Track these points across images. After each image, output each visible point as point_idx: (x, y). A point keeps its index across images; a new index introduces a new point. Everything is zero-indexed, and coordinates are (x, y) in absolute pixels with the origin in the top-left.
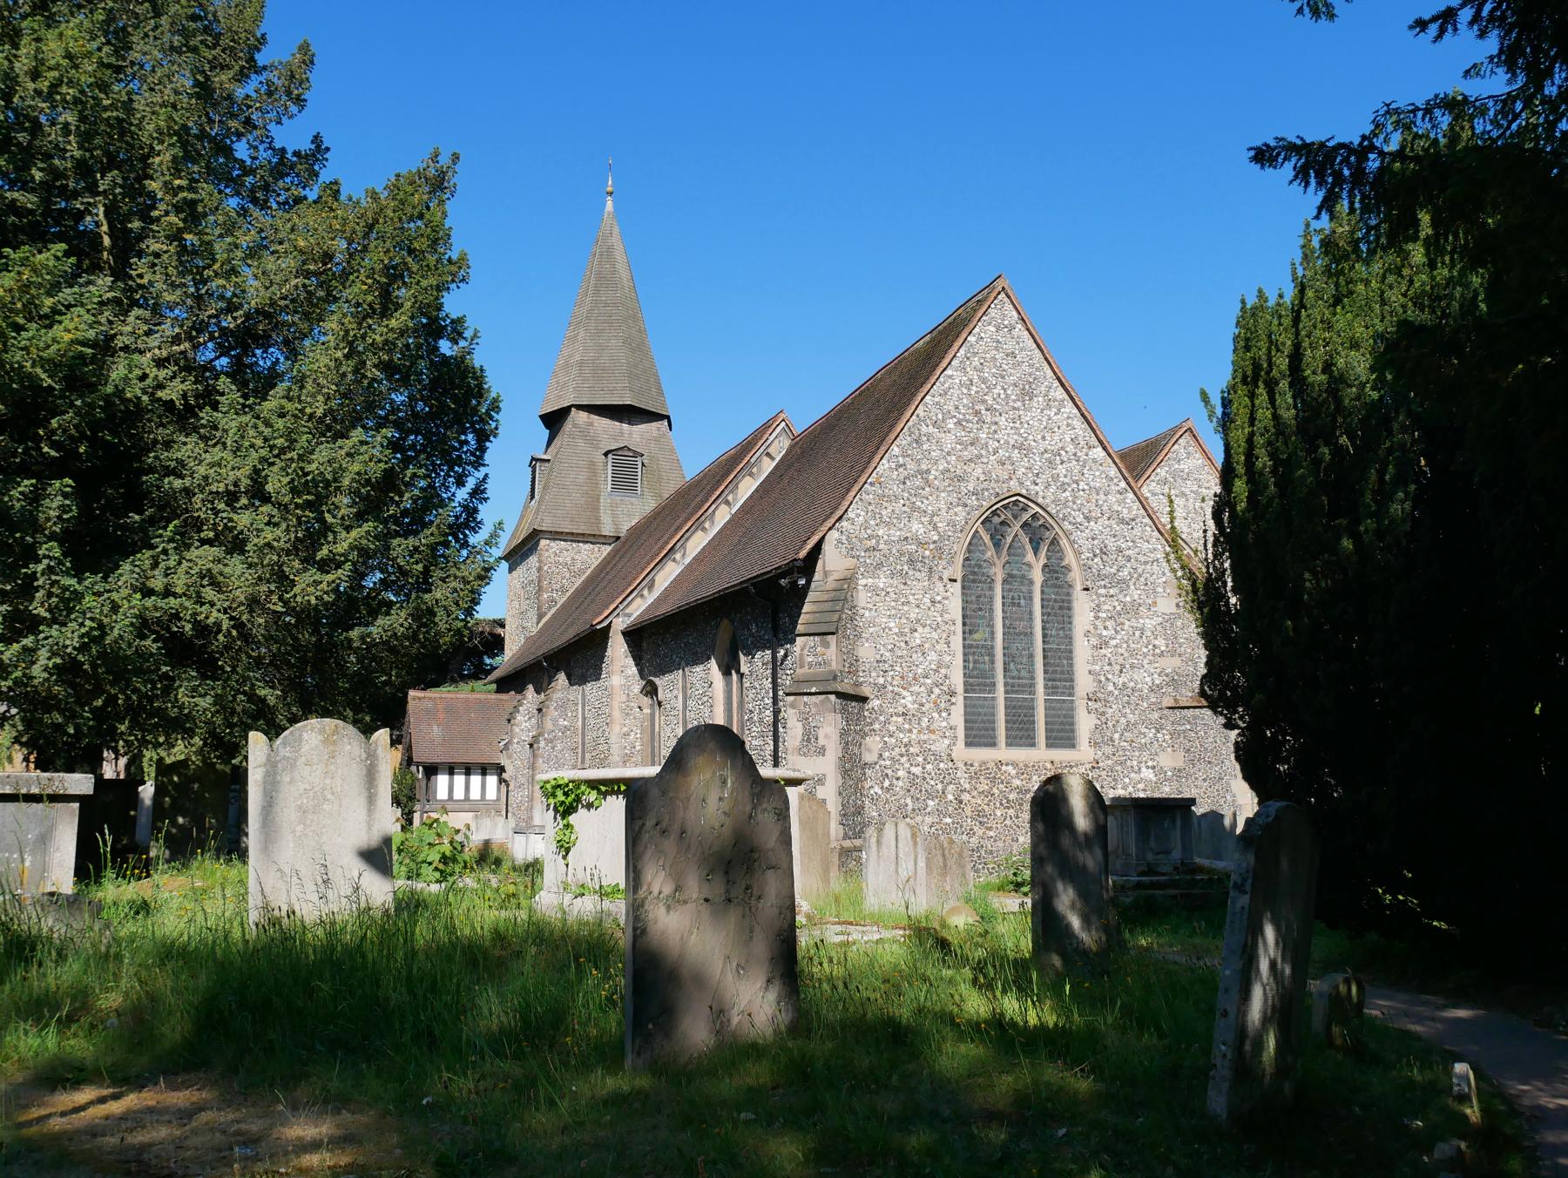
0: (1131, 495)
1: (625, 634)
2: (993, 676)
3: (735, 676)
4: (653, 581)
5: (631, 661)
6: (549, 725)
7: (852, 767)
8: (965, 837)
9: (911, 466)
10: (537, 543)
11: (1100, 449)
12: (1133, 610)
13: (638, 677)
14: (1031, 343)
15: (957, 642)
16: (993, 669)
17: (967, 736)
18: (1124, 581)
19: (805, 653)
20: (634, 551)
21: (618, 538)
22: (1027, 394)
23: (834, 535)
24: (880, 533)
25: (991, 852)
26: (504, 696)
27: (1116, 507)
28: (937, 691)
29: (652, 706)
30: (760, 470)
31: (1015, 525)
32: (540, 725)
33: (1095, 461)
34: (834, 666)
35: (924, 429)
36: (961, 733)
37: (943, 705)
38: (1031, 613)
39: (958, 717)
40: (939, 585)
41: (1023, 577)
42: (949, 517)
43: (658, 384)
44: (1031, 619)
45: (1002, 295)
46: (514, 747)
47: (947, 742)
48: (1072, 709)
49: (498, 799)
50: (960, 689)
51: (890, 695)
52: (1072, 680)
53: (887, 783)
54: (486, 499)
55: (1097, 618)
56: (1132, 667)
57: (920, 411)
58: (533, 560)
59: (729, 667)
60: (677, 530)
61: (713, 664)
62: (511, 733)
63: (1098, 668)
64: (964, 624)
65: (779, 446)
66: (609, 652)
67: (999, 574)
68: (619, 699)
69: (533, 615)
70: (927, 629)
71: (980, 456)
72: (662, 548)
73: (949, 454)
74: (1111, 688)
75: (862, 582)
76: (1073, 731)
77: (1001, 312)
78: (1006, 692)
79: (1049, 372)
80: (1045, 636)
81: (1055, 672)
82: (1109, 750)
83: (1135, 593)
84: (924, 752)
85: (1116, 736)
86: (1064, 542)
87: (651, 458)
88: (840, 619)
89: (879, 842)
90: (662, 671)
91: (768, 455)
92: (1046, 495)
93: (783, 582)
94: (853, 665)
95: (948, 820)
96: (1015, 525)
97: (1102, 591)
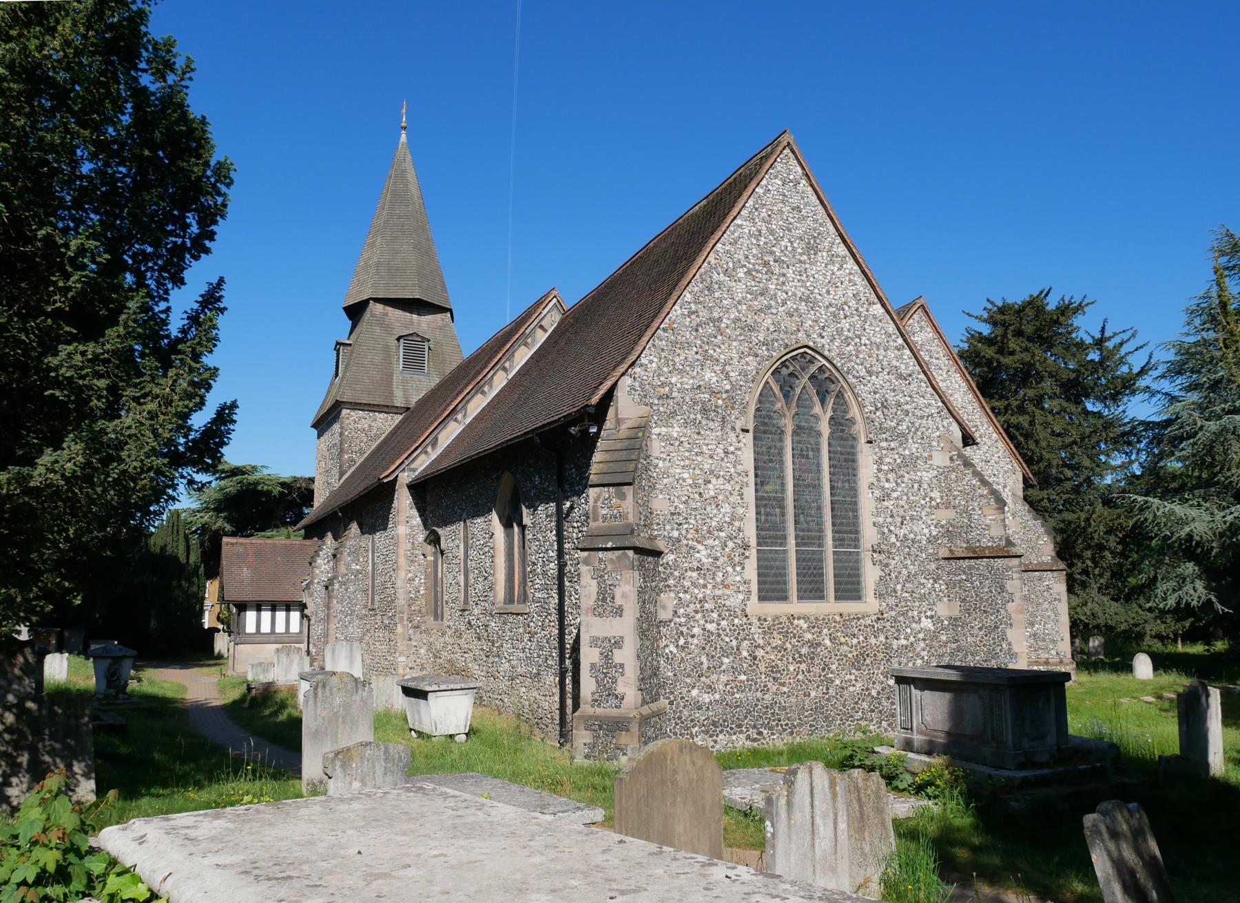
0: (907, 352)
2: (784, 529)
3: (516, 528)
4: (436, 439)
5: (415, 513)
7: (649, 627)
8: (759, 694)
9: (704, 314)
11: (879, 306)
12: (910, 463)
13: (422, 528)
14: (814, 199)
15: (750, 494)
16: (784, 522)
17: (760, 590)
18: (903, 435)
19: (597, 504)
20: (419, 419)
21: (408, 409)
22: (812, 249)
23: (626, 381)
24: (674, 380)
25: (785, 708)
26: (308, 542)
27: (894, 363)
28: (730, 544)
29: (435, 553)
30: (534, 341)
31: (803, 377)
32: (335, 569)
33: (874, 317)
34: (631, 519)
35: (715, 276)
36: (754, 587)
37: (737, 559)
38: (819, 465)
39: (751, 571)
40: (732, 436)
41: (811, 428)
42: (740, 367)
43: (441, 276)
44: (819, 471)
45: (787, 151)
47: (741, 597)
48: (858, 561)
49: (301, 632)
50: (753, 542)
51: (684, 550)
52: (857, 532)
53: (682, 642)
54: (222, 310)
55: (880, 470)
56: (912, 519)
57: (711, 258)
58: (336, 427)
59: (511, 520)
60: (460, 392)
61: (494, 517)
63: (881, 520)
64: (756, 476)
65: (551, 320)
67: (788, 425)
68: (405, 546)
69: (335, 472)
70: (721, 481)
71: (770, 307)
72: (445, 409)
73: (739, 303)
74: (893, 539)
75: (656, 431)
76: (859, 583)
77: (786, 167)
78: (797, 545)
79: (832, 228)
80: (832, 488)
81: (842, 524)
82: (892, 601)
83: (913, 447)
84: (719, 608)
85: (899, 587)
86: (849, 395)
87: (437, 343)
88: (636, 468)
89: (789, 804)
90: (445, 522)
91: (541, 327)
92: (832, 348)
93: (573, 430)
94: (648, 516)
95: (743, 677)
96: (803, 377)
97: (884, 444)
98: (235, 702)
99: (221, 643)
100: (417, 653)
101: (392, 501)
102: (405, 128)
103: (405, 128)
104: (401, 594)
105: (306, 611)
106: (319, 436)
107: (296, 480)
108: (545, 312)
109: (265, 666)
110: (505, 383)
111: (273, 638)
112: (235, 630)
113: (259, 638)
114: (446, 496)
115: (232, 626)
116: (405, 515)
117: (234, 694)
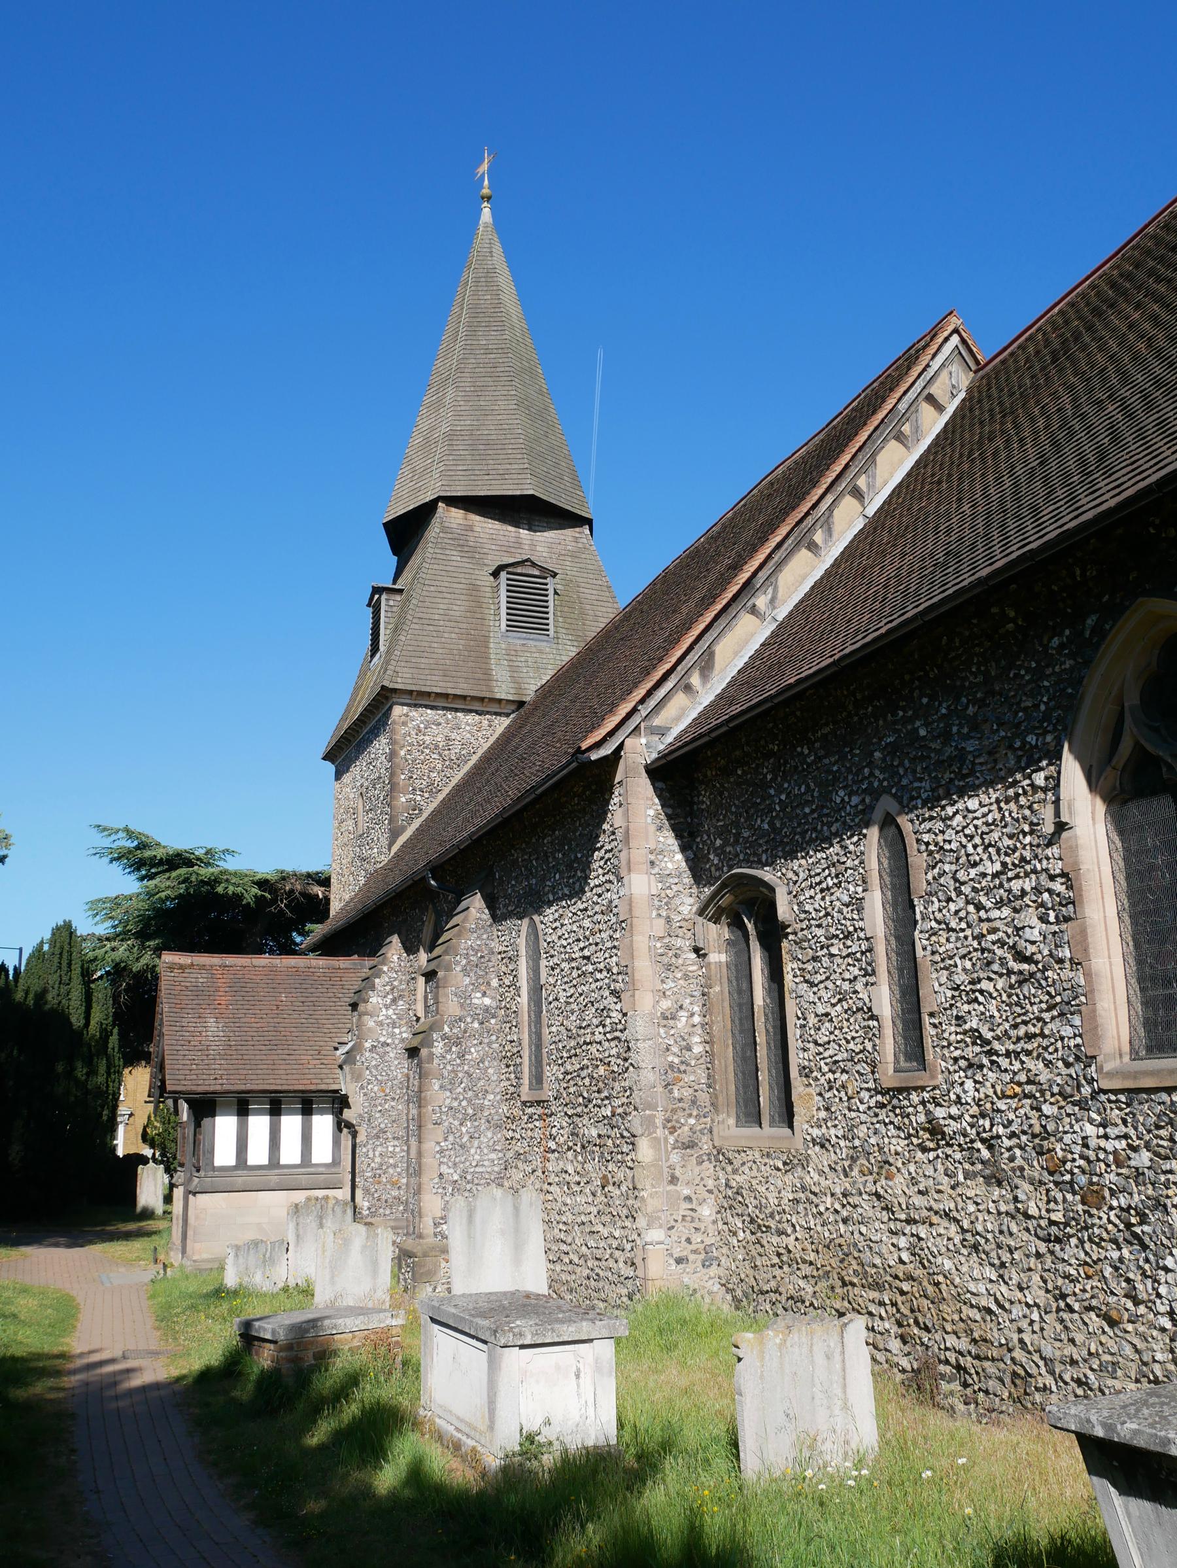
1: (658, 772)
4: (709, 654)
5: (669, 840)
6: (451, 1006)
10: (388, 714)
13: (687, 879)
21: (521, 704)
46: (366, 1057)
49: (336, 1162)
58: (380, 746)
62: (359, 1032)
65: (951, 382)
66: (616, 818)
87: (567, 583)
91: (930, 399)
98: (206, 1376)
99: (150, 1187)
100: (691, 1217)
101: (602, 814)
102: (489, 198)
103: (489, 198)
104: (645, 1055)
105: (347, 1114)
106: (338, 776)
107: (284, 877)
108: (936, 364)
109: (266, 1249)
110: (859, 524)
111: (273, 1178)
112: (188, 1160)
113: (244, 1178)
114: (757, 785)
115: (177, 1150)
116: (644, 854)
117: (206, 1346)
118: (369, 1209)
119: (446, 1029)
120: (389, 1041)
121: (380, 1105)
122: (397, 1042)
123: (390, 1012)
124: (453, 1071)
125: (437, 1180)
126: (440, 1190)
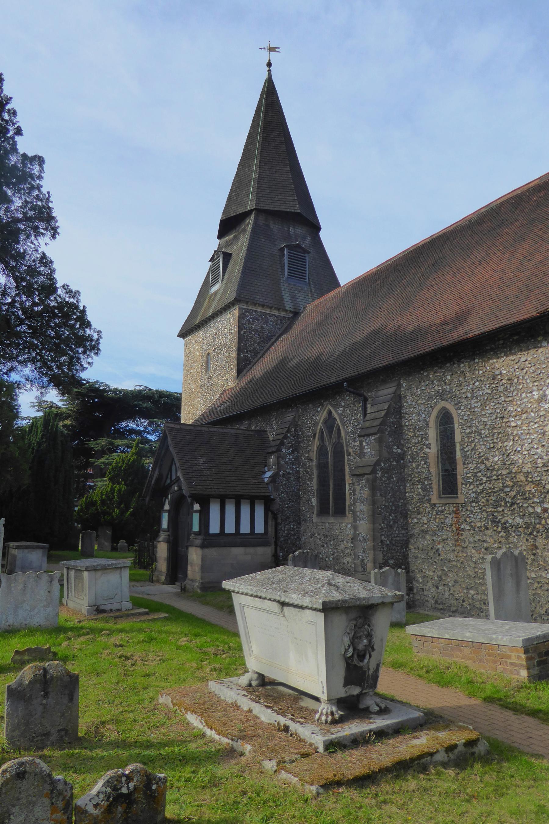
118: (283, 556)
119: (383, 465)
120: (291, 472)
121: (287, 504)
122: (294, 472)
123: (291, 457)
124: (385, 487)
125: (380, 544)
126: (382, 549)
